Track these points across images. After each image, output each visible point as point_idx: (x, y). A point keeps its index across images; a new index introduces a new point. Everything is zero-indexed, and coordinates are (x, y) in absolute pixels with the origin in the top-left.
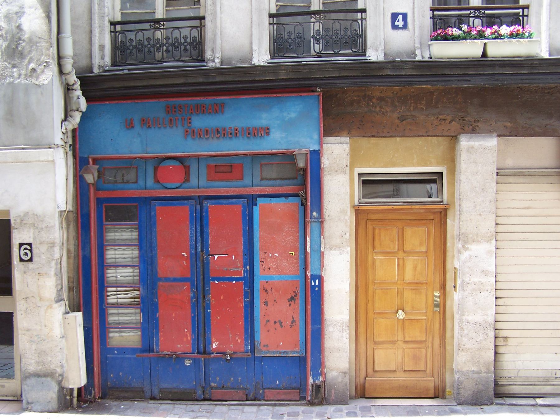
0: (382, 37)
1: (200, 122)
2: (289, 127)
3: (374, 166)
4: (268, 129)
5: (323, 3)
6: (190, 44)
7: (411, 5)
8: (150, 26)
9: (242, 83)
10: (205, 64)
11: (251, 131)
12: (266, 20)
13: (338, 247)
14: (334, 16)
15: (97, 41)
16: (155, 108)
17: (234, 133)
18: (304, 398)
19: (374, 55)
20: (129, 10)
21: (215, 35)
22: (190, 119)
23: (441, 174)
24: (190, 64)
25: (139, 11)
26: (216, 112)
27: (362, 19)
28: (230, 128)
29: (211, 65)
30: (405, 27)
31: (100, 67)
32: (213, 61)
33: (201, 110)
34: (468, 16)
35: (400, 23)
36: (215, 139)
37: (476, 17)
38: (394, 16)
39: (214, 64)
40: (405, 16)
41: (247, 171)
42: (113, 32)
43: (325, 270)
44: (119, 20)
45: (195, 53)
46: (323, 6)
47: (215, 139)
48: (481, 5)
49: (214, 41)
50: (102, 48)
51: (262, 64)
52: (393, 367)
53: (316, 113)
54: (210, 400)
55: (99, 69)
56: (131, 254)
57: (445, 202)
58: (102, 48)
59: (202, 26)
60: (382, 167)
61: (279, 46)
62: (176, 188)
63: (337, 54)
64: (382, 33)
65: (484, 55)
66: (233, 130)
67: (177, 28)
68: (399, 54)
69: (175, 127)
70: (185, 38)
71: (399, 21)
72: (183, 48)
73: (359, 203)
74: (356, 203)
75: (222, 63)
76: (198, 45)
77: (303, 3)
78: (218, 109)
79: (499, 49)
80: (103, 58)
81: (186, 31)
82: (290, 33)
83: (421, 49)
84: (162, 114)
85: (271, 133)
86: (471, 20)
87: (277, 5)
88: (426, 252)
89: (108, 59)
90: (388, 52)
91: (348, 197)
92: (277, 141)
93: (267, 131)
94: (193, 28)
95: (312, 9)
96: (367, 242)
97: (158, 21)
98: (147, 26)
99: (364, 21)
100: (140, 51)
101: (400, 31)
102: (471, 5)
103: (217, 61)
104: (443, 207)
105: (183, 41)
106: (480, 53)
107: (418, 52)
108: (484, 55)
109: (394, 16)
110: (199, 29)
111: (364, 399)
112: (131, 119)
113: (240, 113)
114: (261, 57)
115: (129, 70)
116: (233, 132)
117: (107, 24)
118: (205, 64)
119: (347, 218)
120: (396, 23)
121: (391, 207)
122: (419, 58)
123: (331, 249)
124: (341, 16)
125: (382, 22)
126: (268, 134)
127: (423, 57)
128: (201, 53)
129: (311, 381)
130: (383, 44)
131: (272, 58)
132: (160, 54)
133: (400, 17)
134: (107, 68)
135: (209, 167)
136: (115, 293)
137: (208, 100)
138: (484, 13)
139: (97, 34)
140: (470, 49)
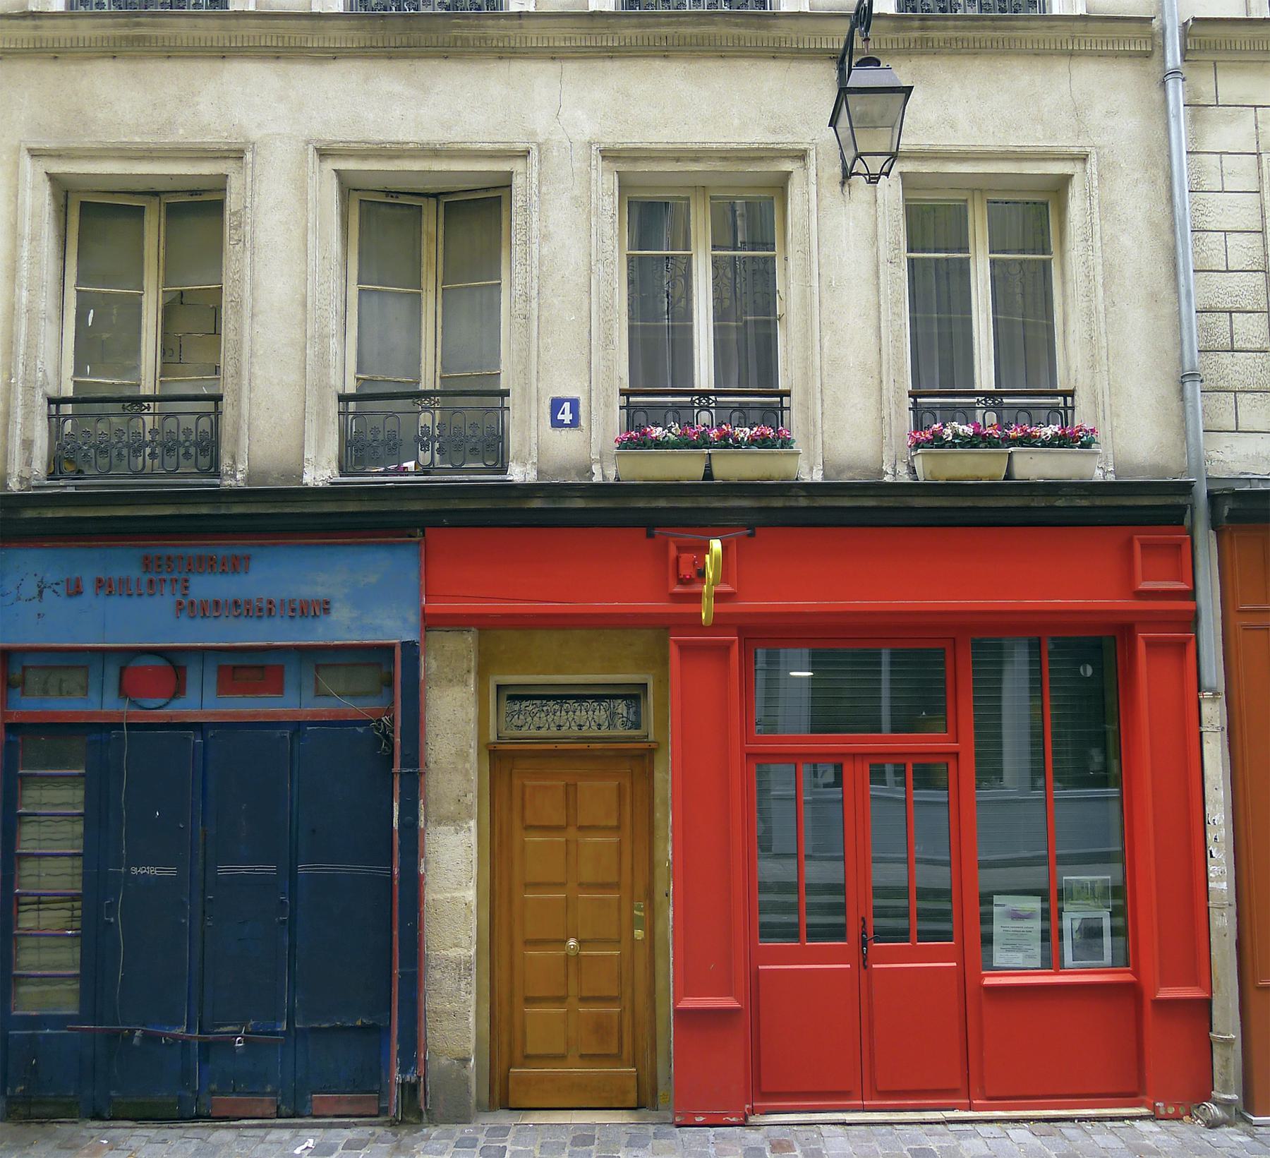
0: (534, 440)
1: (205, 586)
2: (364, 600)
3: (525, 671)
4: (327, 603)
5: (441, 378)
6: (196, 444)
7: (586, 384)
8: (124, 408)
9: (286, 517)
10: (217, 481)
11: (297, 605)
12: (333, 407)
13: (454, 820)
14: (461, 401)
15: (18, 432)
16: (123, 563)
17: (266, 610)
18: (383, 1111)
19: (518, 473)
20: (90, 376)
21: (237, 428)
22: (186, 581)
23: (644, 686)
24: (190, 481)
25: (106, 381)
26: (235, 570)
27: (1066, 407)
28: (260, 600)
29: (228, 483)
30: (575, 423)
31: (22, 480)
32: (234, 476)
33: (208, 565)
34: (972, 407)
35: (567, 417)
36: (231, 617)
37: (988, 409)
38: (556, 404)
39: (233, 483)
40: (575, 404)
41: (289, 679)
42: (55, 420)
43: (432, 866)
44: (71, 394)
45: (204, 462)
46: (442, 383)
47: (231, 617)
48: (993, 388)
49: (236, 441)
50: (28, 444)
51: (321, 485)
52: (559, 1049)
53: (413, 575)
54: (208, 1117)
55: (21, 483)
56: (69, 837)
57: (651, 738)
58: (28, 444)
59: (218, 413)
60: (538, 674)
61: (354, 451)
62: (160, 708)
63: (457, 470)
64: (534, 434)
65: (708, 475)
66: (265, 601)
67: (174, 415)
68: (564, 470)
69: (158, 594)
70: (187, 431)
71: (564, 413)
72: (182, 451)
73: (498, 738)
74: (493, 737)
75: (249, 478)
76: (209, 447)
77: (407, 376)
78: (237, 565)
79: (731, 467)
80: (28, 463)
81: (188, 419)
82: (375, 430)
83: (602, 463)
84: (134, 572)
85: (333, 611)
86: (979, 413)
87: (358, 379)
88: (618, 828)
89: (39, 466)
90: (544, 467)
91: (472, 728)
92: (343, 627)
93: (325, 607)
94: (201, 415)
95: (422, 387)
96: (511, 809)
97: (138, 401)
98: (117, 408)
99: (1069, 412)
100: (104, 452)
101: (565, 431)
102: (977, 388)
103: (239, 476)
104: (646, 746)
105: (182, 438)
106: (700, 471)
107: (596, 468)
108: (708, 475)
109: (556, 404)
110: (213, 417)
111: (507, 1112)
112: (78, 580)
113: (279, 574)
114: (320, 470)
115: (76, 487)
116: (265, 605)
117: (40, 401)
118: (217, 481)
119: (468, 766)
120: (560, 417)
121: (552, 747)
122: (597, 479)
123: (439, 824)
124: (474, 401)
125: (534, 415)
126: (327, 611)
127: (604, 476)
128: (216, 462)
129: (397, 1077)
130: (534, 453)
131: (343, 471)
132: (141, 459)
133: (567, 405)
134: (34, 483)
135: (221, 669)
136: (35, 907)
137: (221, 550)
138: (715, 401)
139: (19, 420)
140: (687, 467)
